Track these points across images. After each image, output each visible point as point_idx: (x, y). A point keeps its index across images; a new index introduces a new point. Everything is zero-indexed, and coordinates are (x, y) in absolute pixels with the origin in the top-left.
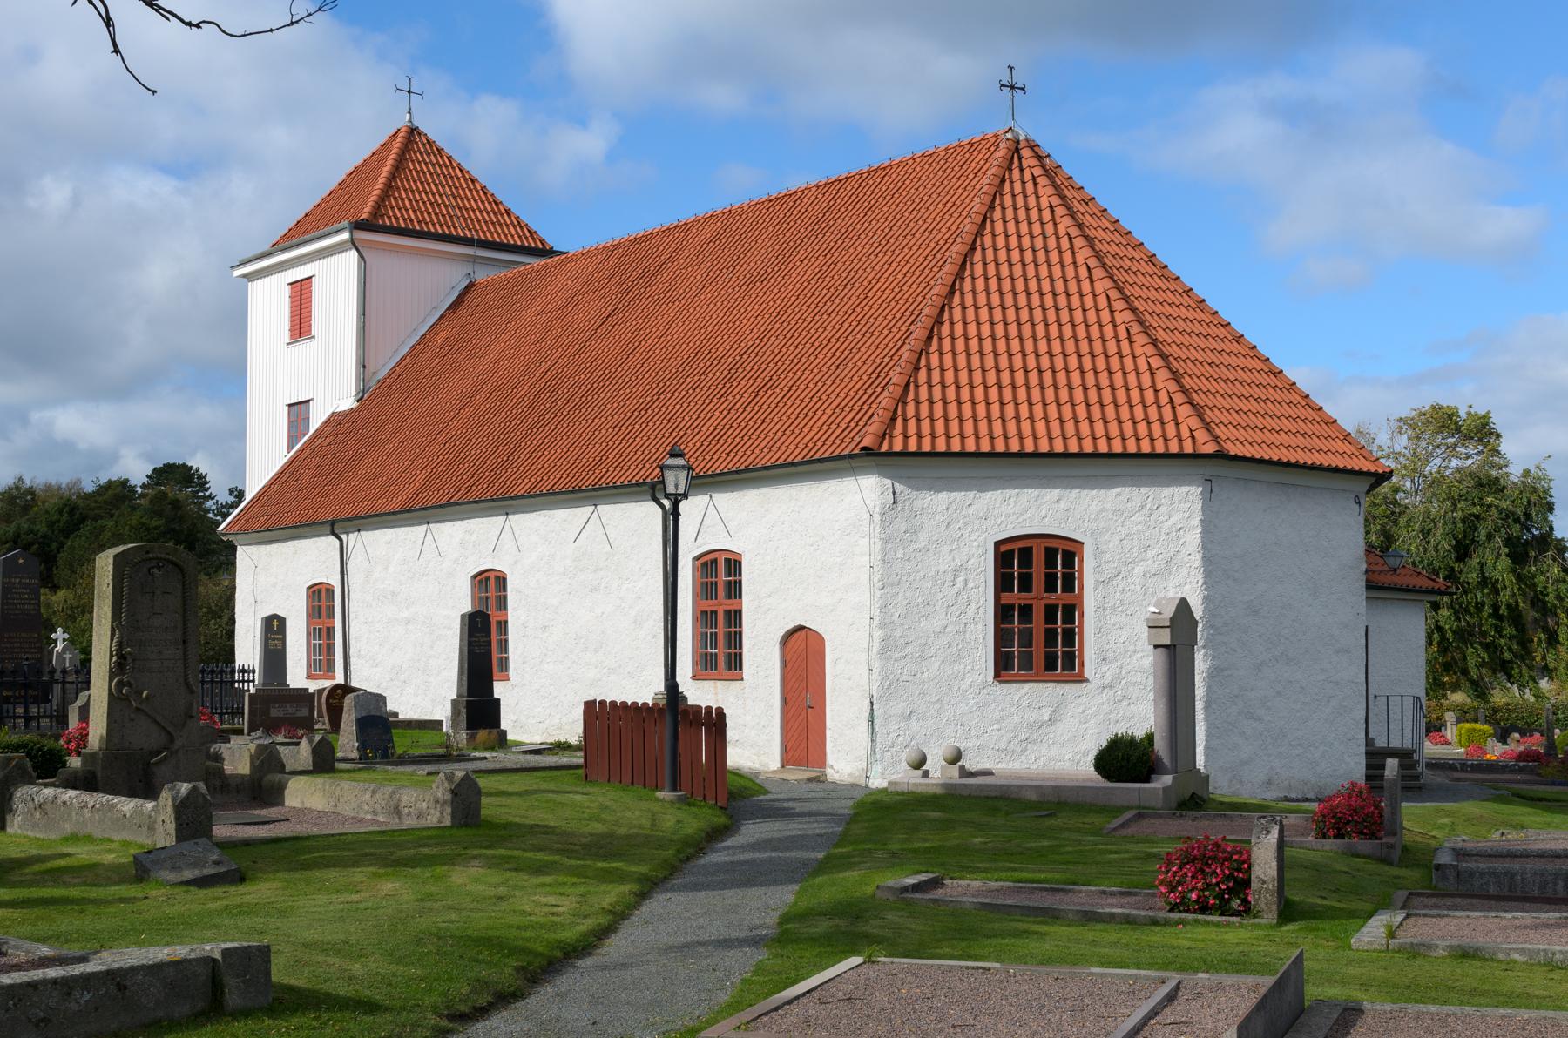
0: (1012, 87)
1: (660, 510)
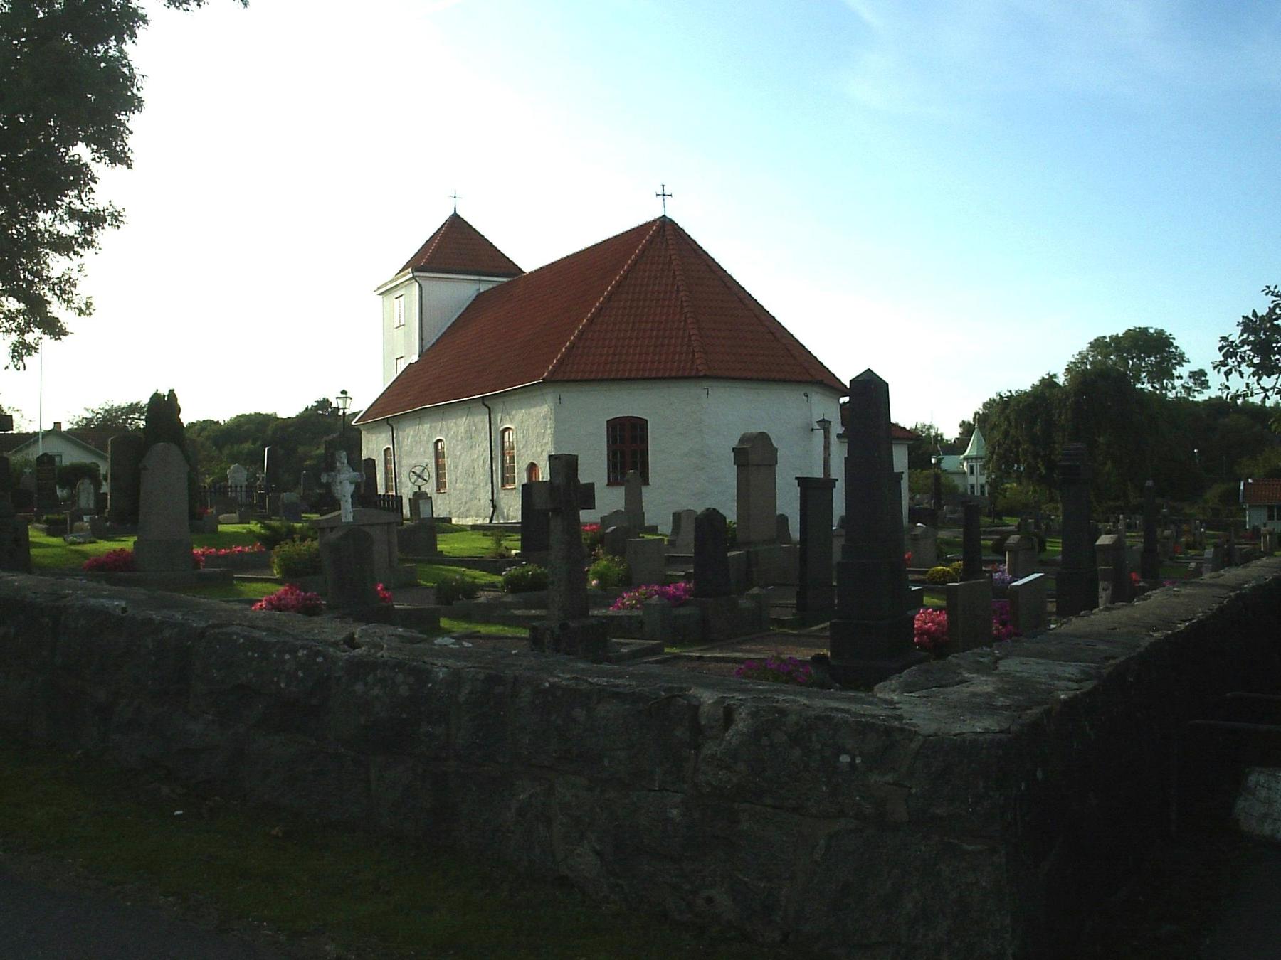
0: (664, 195)
1: (487, 410)
